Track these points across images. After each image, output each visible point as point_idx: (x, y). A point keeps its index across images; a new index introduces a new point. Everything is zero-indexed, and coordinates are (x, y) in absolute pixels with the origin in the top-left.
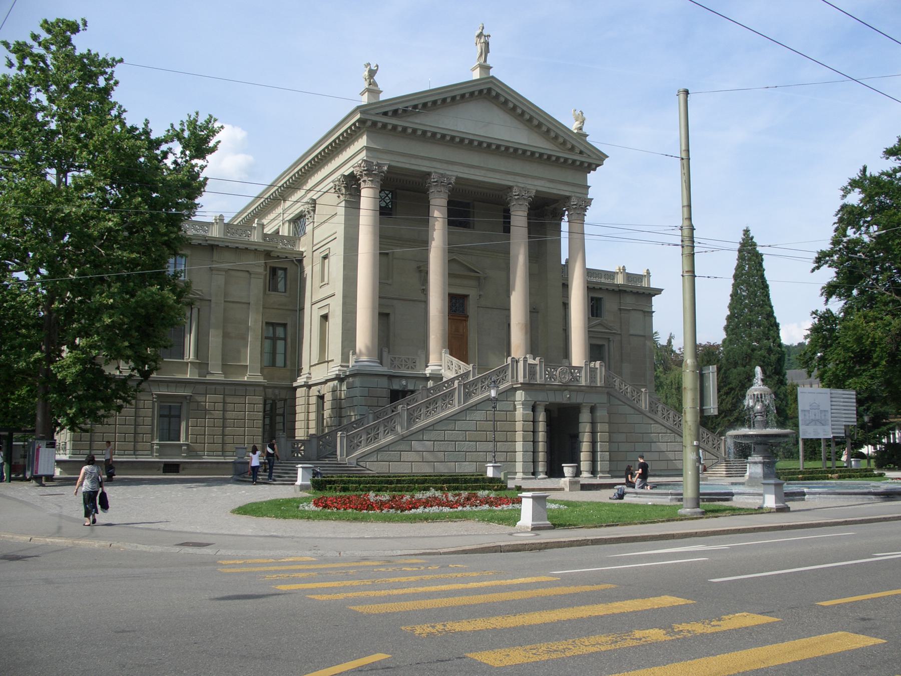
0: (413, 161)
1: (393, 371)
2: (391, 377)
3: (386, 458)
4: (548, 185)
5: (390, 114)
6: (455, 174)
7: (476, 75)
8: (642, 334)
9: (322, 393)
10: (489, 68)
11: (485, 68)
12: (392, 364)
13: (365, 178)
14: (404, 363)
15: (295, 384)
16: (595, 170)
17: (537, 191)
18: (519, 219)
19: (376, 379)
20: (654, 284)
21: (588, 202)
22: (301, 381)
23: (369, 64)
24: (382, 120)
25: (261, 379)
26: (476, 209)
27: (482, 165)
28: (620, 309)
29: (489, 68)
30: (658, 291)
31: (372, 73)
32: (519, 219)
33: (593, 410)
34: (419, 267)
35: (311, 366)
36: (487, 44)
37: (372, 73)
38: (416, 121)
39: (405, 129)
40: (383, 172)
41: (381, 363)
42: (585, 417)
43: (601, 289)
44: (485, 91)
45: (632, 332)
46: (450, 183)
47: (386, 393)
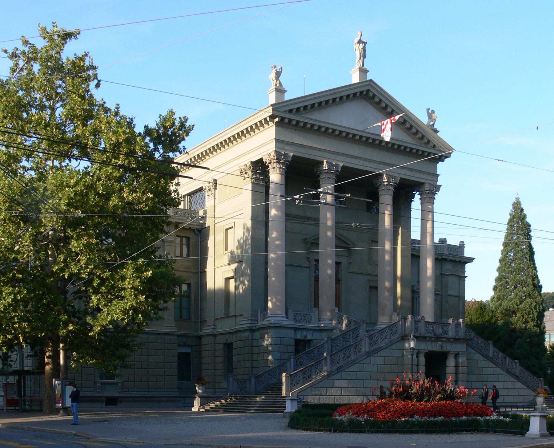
0: (310, 152)
1: (298, 325)
2: (296, 329)
3: (317, 393)
4: (408, 173)
5: (294, 111)
6: (400, 176)
7: (355, 79)
8: (457, 295)
9: (229, 341)
10: (366, 71)
11: (363, 71)
12: (294, 319)
13: (274, 165)
14: (303, 318)
15: (200, 333)
16: (443, 161)
17: (401, 178)
18: (386, 200)
19: (285, 331)
20: (467, 254)
21: (438, 188)
22: (207, 330)
23: (275, 67)
24: (291, 116)
25: (175, 330)
26: (359, 189)
27: (361, 156)
28: (442, 274)
29: (366, 71)
30: (471, 260)
31: (278, 74)
32: (386, 200)
33: (456, 356)
34: (304, 239)
35: (215, 320)
36: (364, 49)
37: (278, 74)
38: (313, 117)
39: (298, 122)
40: (288, 161)
41: (287, 318)
42: (451, 362)
43: (460, 261)
44: (365, 93)
45: (449, 293)
46: (338, 171)
47: (292, 342)
